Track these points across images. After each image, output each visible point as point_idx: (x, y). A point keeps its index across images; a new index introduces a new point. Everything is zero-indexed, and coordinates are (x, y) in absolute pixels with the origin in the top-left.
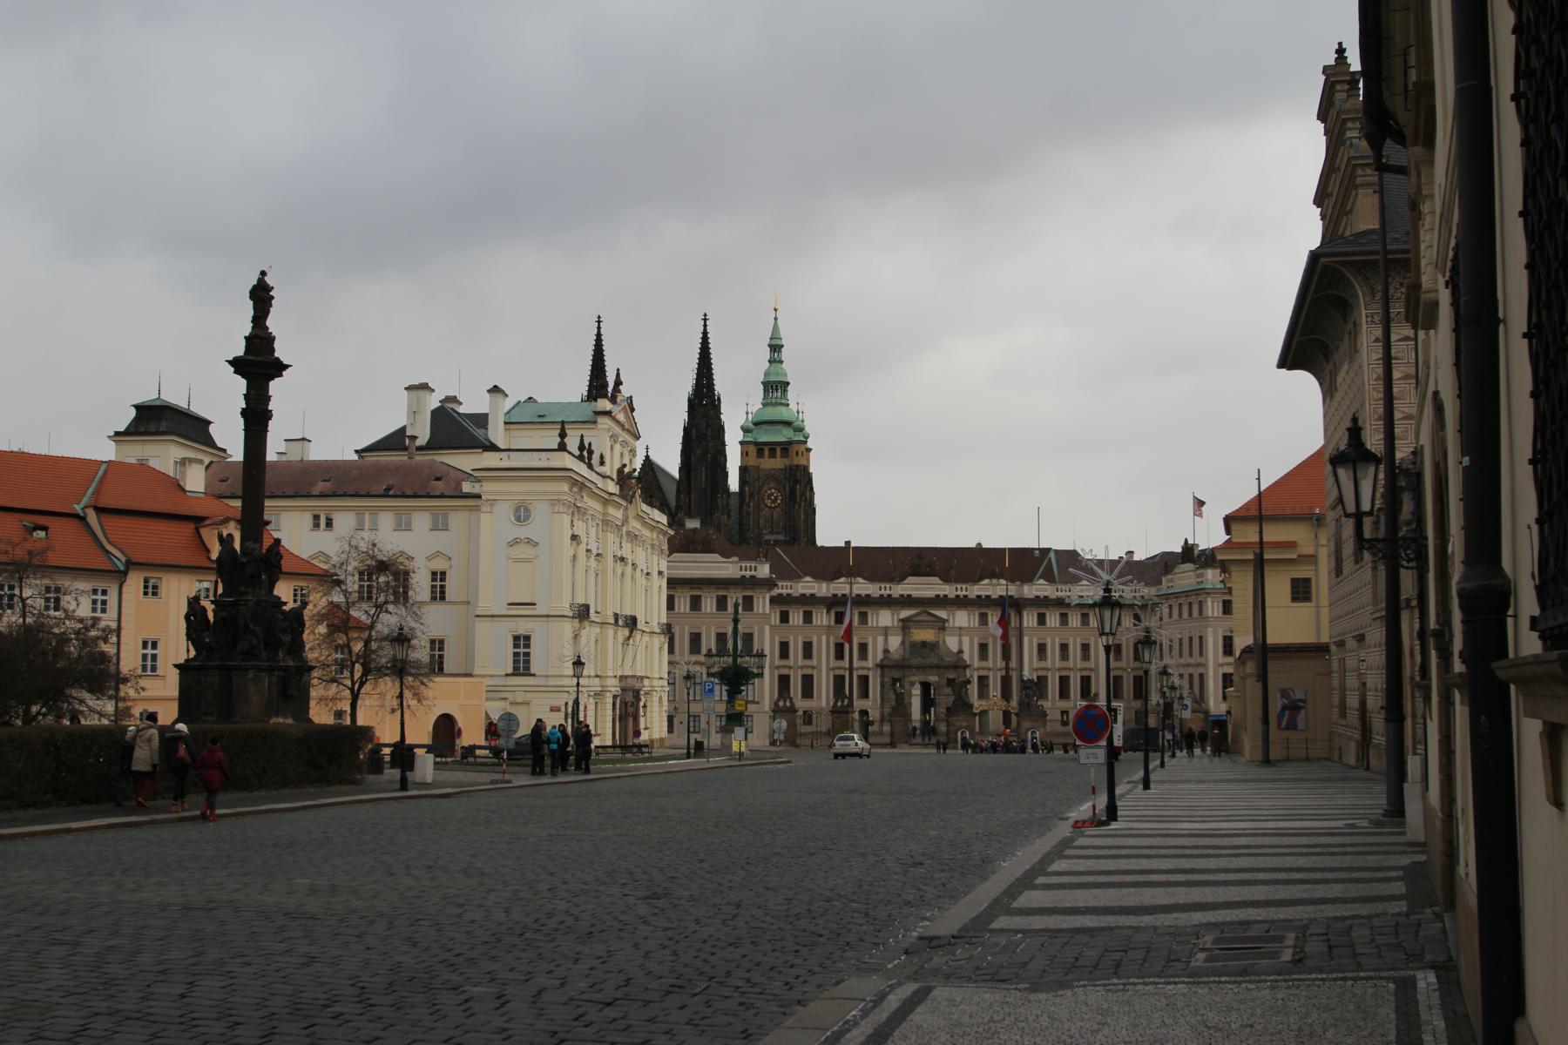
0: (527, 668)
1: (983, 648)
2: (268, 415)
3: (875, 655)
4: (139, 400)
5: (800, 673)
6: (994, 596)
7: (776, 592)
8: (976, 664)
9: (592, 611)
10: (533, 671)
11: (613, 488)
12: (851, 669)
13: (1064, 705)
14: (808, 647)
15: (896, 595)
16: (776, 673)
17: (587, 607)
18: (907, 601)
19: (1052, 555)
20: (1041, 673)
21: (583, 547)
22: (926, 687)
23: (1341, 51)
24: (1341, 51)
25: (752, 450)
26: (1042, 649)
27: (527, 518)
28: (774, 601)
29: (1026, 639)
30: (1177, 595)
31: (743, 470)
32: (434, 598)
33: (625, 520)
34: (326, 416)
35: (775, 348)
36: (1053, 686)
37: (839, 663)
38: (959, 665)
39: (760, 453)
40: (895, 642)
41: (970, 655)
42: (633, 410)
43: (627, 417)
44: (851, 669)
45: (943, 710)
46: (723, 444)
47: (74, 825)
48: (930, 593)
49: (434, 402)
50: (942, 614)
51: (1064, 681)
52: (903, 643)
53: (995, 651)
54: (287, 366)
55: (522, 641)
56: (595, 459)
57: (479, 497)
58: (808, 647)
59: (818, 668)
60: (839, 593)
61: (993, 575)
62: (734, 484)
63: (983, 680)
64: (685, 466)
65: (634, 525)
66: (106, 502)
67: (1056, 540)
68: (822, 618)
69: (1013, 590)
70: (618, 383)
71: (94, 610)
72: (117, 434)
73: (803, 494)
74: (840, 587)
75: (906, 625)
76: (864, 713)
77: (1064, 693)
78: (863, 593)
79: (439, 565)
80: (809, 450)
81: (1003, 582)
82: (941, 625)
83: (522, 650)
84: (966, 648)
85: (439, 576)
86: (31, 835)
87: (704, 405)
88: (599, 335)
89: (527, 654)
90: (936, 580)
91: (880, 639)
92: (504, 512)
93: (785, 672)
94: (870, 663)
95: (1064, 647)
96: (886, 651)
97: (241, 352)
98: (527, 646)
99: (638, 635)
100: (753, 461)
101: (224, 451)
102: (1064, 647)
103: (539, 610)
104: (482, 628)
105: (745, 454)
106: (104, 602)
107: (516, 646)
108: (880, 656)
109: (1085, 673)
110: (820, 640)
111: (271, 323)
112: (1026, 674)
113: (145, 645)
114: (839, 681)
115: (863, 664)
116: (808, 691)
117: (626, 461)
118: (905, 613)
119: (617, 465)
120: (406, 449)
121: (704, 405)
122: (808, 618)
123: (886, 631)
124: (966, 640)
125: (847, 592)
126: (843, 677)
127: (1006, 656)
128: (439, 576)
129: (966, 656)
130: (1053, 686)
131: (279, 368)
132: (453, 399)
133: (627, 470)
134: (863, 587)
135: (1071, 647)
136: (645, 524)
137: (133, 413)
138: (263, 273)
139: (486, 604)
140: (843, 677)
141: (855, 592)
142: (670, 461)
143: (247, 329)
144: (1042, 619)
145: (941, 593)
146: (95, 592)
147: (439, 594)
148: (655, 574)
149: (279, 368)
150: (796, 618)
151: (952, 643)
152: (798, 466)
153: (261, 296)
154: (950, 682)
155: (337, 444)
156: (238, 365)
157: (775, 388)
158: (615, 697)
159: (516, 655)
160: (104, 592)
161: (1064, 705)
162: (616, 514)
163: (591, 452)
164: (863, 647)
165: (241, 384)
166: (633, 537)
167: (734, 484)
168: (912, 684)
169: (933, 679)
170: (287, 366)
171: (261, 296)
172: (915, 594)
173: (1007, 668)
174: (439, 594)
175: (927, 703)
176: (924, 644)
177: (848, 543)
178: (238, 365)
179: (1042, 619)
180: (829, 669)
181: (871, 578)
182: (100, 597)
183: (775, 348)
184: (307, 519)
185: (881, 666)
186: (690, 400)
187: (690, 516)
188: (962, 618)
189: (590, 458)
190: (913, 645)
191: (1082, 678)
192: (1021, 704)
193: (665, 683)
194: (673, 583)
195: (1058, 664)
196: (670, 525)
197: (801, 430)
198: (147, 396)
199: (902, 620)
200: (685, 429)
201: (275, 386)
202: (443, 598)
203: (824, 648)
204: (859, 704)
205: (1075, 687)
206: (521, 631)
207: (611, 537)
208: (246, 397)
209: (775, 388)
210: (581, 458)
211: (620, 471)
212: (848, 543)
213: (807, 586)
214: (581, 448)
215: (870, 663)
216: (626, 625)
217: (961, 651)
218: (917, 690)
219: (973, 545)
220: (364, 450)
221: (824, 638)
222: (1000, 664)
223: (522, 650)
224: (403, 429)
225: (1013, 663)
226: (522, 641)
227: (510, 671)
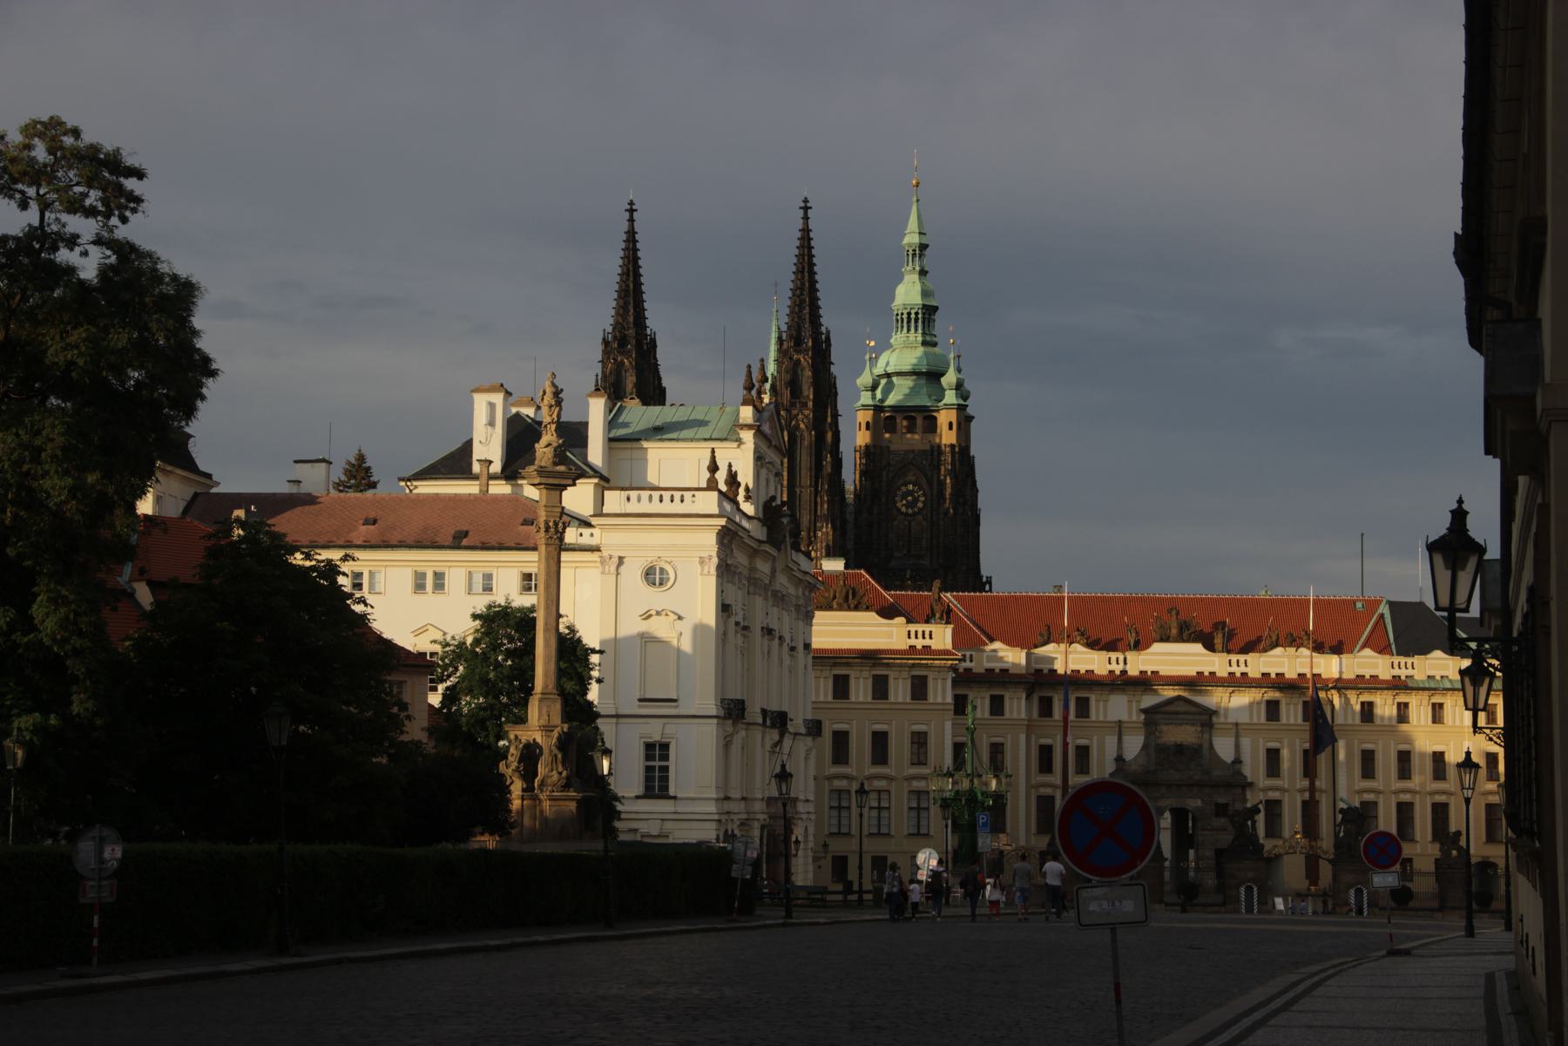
0: (664, 787)
1: (1273, 756)
5: (1394, 801)
8: (1262, 781)
10: (672, 792)
15: (1133, 671)
16: (827, 787)
19: (1384, 609)
21: (732, 620)
22: (1180, 815)
23: (1459, 515)
24: (1459, 515)
38: (1235, 781)
40: (1133, 745)
41: (1253, 768)
45: (1209, 853)
52: (1145, 747)
53: (1290, 759)
57: (597, 549)
61: (1294, 641)
63: (1273, 807)
65: (782, 580)
68: (1018, 706)
78: (1083, 669)
81: (1304, 651)
83: (657, 763)
84: (1246, 756)
86: (383, 958)
89: (665, 769)
90: (1198, 648)
91: (1111, 742)
93: (1406, 798)
96: (1119, 759)
98: (665, 757)
99: (787, 742)
101: (209, 476)
107: (649, 757)
112: (1342, 792)
120: (476, 478)
122: (997, 706)
124: (1246, 742)
126: (1051, 799)
127: (1309, 770)
140: (1051, 799)
145: (1207, 671)
148: (801, 648)
150: (980, 703)
151: (1224, 748)
154: (1221, 810)
158: (763, 827)
159: (649, 769)
162: (764, 567)
164: (1083, 752)
168: (1161, 812)
169: (1194, 803)
173: (1312, 789)
175: (1183, 840)
176: (1180, 749)
180: (1029, 787)
181: (1093, 645)
190: (1163, 750)
191: (1435, 805)
192: (1338, 844)
199: (1145, 711)
203: (1020, 756)
207: (759, 601)
216: (773, 726)
217: (1238, 761)
218: (1166, 821)
221: (1023, 737)
223: (657, 763)
225: (1322, 783)
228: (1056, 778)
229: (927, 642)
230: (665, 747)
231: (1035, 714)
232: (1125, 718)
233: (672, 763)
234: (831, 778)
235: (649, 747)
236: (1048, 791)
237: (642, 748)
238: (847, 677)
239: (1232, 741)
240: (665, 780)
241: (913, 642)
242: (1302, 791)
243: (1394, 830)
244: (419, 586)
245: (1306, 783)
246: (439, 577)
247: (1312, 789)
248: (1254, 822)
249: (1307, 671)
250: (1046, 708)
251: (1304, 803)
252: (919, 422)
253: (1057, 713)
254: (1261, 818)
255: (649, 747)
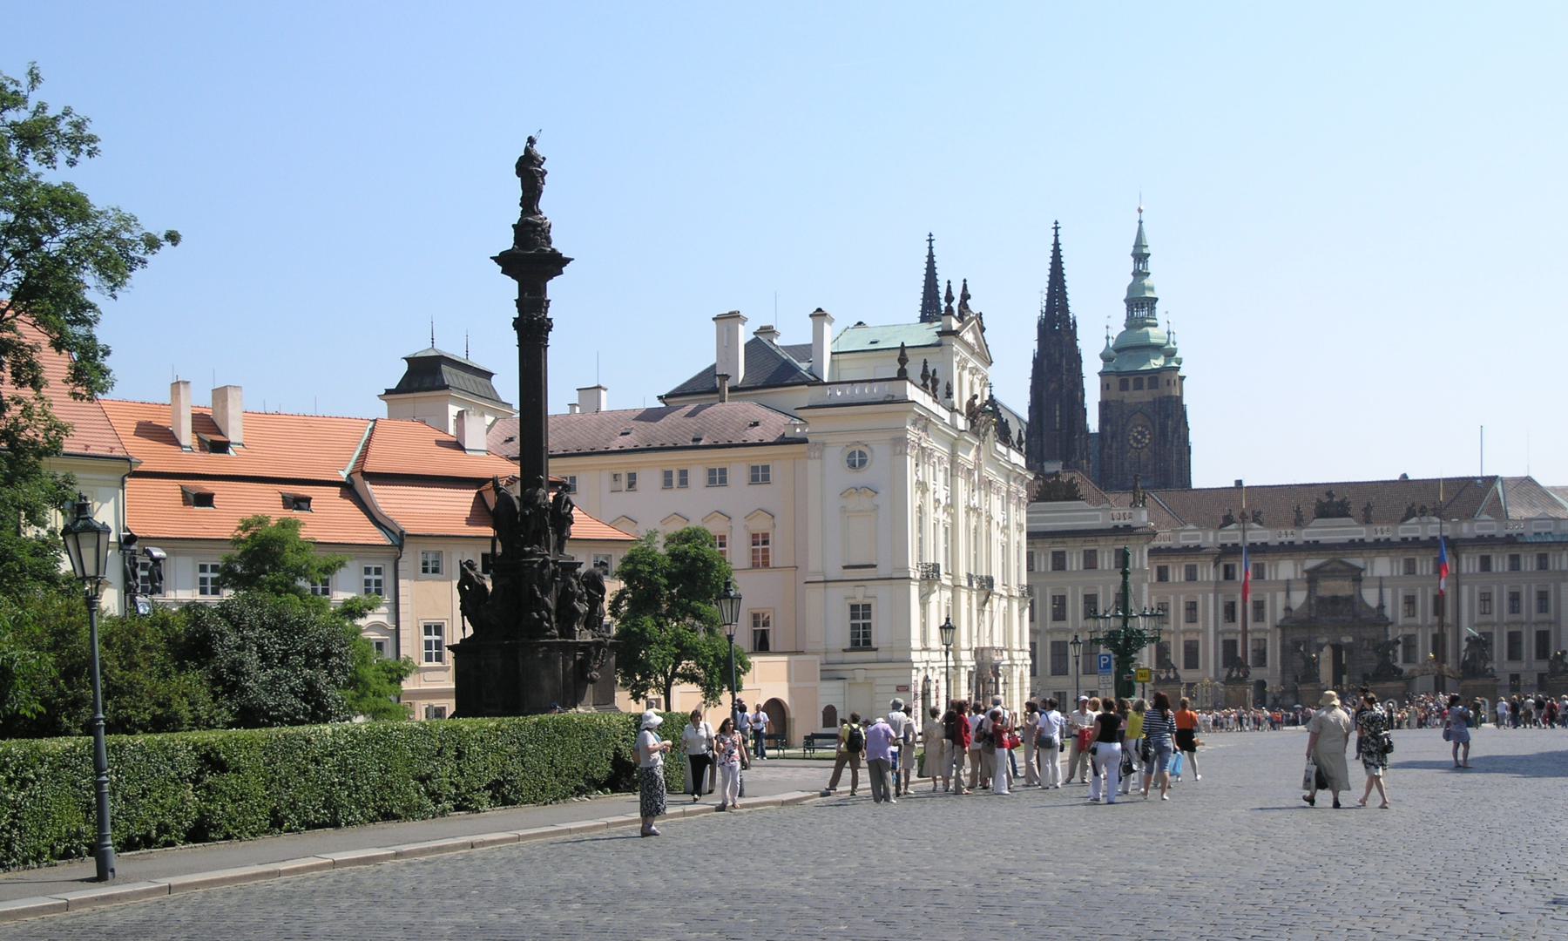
0: (868, 643)
1: (1410, 601)
2: (547, 326)
3: (1276, 609)
4: (410, 353)
6: (1424, 538)
7: (1156, 543)
9: (942, 571)
10: (874, 645)
11: (962, 423)
12: (1245, 632)
13: (1514, 667)
14: (1192, 608)
15: (1395, 539)
17: (936, 567)
18: (1314, 547)
20: (1486, 629)
21: (930, 497)
22: (1337, 649)
25: (1115, 381)
26: (1486, 598)
27: (863, 463)
28: (1155, 552)
29: (1465, 590)
30: (1510, 541)
31: (1104, 406)
32: (755, 566)
33: (978, 466)
34: (622, 351)
35: (1140, 256)
36: (1500, 646)
37: (1231, 626)
38: (1379, 619)
39: (1124, 386)
40: (1299, 598)
41: (1394, 609)
42: (983, 330)
43: (976, 338)
44: (1245, 632)
46: (1080, 376)
47: (339, 857)
48: (1344, 538)
49: (745, 334)
50: (1358, 562)
51: (1514, 640)
52: (1309, 597)
54: (568, 260)
55: (860, 612)
56: (941, 387)
58: (1192, 608)
59: (1205, 631)
60: (1229, 542)
62: (1093, 423)
63: (1409, 643)
64: (1034, 408)
65: (990, 472)
66: (370, 467)
67: (1504, 466)
69: (1449, 530)
70: (965, 296)
71: (367, 591)
72: (388, 392)
73: (1176, 430)
74: (1232, 535)
75: (1313, 577)
76: (1261, 684)
77: (1514, 653)
78: (1258, 540)
79: (761, 525)
80: (1182, 378)
82: (1356, 576)
83: (861, 622)
85: (760, 540)
87: (1056, 330)
88: (931, 256)
91: (1281, 596)
92: (835, 456)
93: (1193, 637)
94: (1268, 624)
95: (1515, 598)
96: (1288, 609)
97: (508, 244)
100: (1115, 394)
102: (1515, 598)
103: (882, 571)
104: (814, 595)
105: (1105, 387)
106: (378, 583)
107: (854, 617)
108: (1280, 615)
109: (1514, 629)
110: (1206, 599)
111: (547, 205)
113: (428, 630)
114: (1230, 646)
115: (1259, 625)
116: (1192, 660)
117: (977, 391)
118: (1311, 563)
119: (967, 397)
121: (1056, 330)
123: (1288, 586)
124: (1388, 593)
125: (1238, 540)
126: (1234, 642)
128: (760, 540)
129: (1388, 612)
130: (1500, 646)
131: (557, 263)
132: (767, 330)
133: (978, 402)
134: (1258, 534)
135: (1419, 601)
136: (999, 468)
137: (404, 367)
138: (531, 141)
139: (814, 565)
140: (1234, 642)
141: (1249, 540)
142: (1016, 398)
143: (515, 214)
144: (1486, 564)
145: (1357, 537)
146: (367, 571)
147: (761, 561)
149: (557, 263)
151: (1370, 597)
152: (1170, 397)
153: (530, 171)
155: (635, 388)
156: (507, 262)
157: (1140, 304)
158: (970, 673)
159: (854, 626)
160: (378, 571)
161: (1514, 667)
163: (935, 382)
164: (1259, 606)
165: (511, 287)
166: (988, 485)
167: (1093, 423)
168: (1320, 648)
170: (568, 260)
171: (530, 171)
172: (1323, 539)
173: (1441, 625)
174: (761, 561)
176: (1335, 600)
177: (1239, 483)
178: (507, 262)
179: (1486, 564)
180: (1217, 633)
182: (373, 577)
183: (1140, 256)
184: (606, 478)
185: (1282, 627)
186: (1040, 325)
187: (1053, 458)
188: (1382, 566)
189: (934, 389)
190: (1321, 600)
191: (1538, 633)
193: (1027, 655)
194: (1032, 536)
195: (1535, 617)
196: (1029, 467)
197: (1170, 354)
198: (420, 348)
200: (1035, 361)
201: (554, 287)
202: (766, 565)
203: (1210, 608)
204: (1256, 674)
205: (1529, 645)
206: (860, 600)
208: (519, 303)
209: (1140, 304)
210: (924, 387)
211: (971, 404)
212: (1239, 483)
213: (1190, 535)
214: (925, 375)
215: (1268, 624)
217: (1381, 606)
218: (1327, 653)
219: (1397, 478)
220: (668, 396)
221: (1211, 596)
222: (1431, 619)
224: (714, 367)
225: (1449, 619)
226: (860, 612)
227: (848, 645)
228: (1239, 625)
229: (1128, 522)
230: (868, 607)
231: (1221, 578)
232: (1292, 576)
233: (873, 621)
234: (1223, 633)
235: (854, 608)
236: (1232, 637)
237: (848, 609)
238: (1063, 553)
239: (1377, 591)
240: (867, 635)
241: (1116, 522)
242: (1431, 626)
243: (470, 494)
244: (668, 483)
245: (1436, 619)
246: (684, 474)
247: (1441, 625)
248: (1395, 652)
249: (1437, 534)
250: (1229, 574)
251: (1435, 636)
252: (1146, 382)
253: (1239, 575)
254: (1400, 648)
255: (854, 608)
